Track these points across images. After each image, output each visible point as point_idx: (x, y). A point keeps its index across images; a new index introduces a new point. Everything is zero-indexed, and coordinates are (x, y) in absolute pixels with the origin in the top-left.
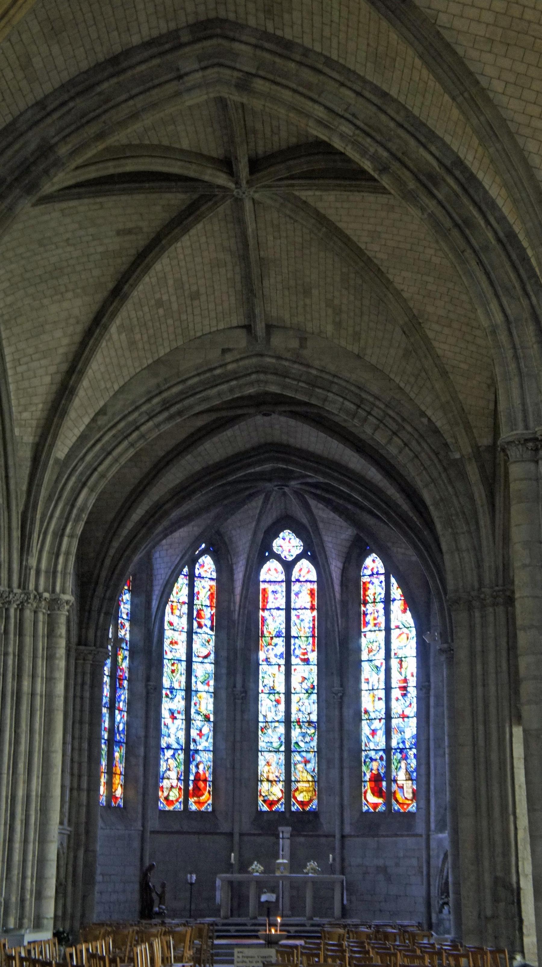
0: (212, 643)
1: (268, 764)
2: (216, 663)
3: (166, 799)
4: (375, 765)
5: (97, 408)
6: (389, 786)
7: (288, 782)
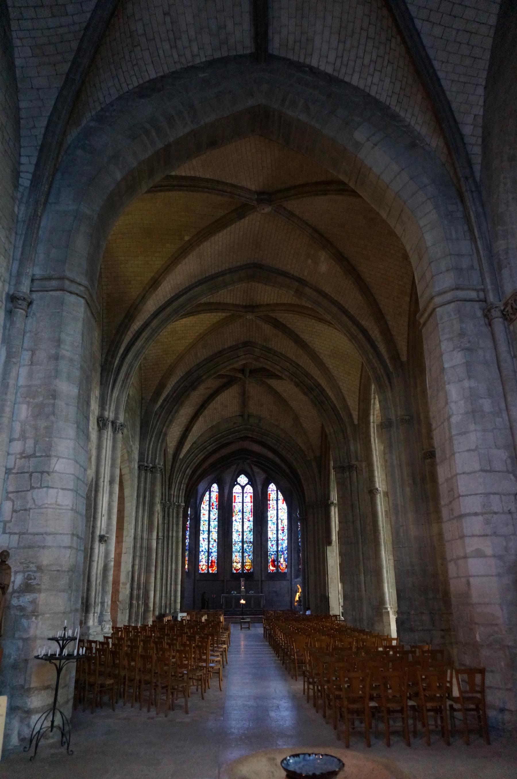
0: (217, 514)
1: (236, 556)
2: (218, 522)
3: (202, 569)
4: (273, 556)
5: (193, 442)
6: (278, 563)
7: (243, 563)
